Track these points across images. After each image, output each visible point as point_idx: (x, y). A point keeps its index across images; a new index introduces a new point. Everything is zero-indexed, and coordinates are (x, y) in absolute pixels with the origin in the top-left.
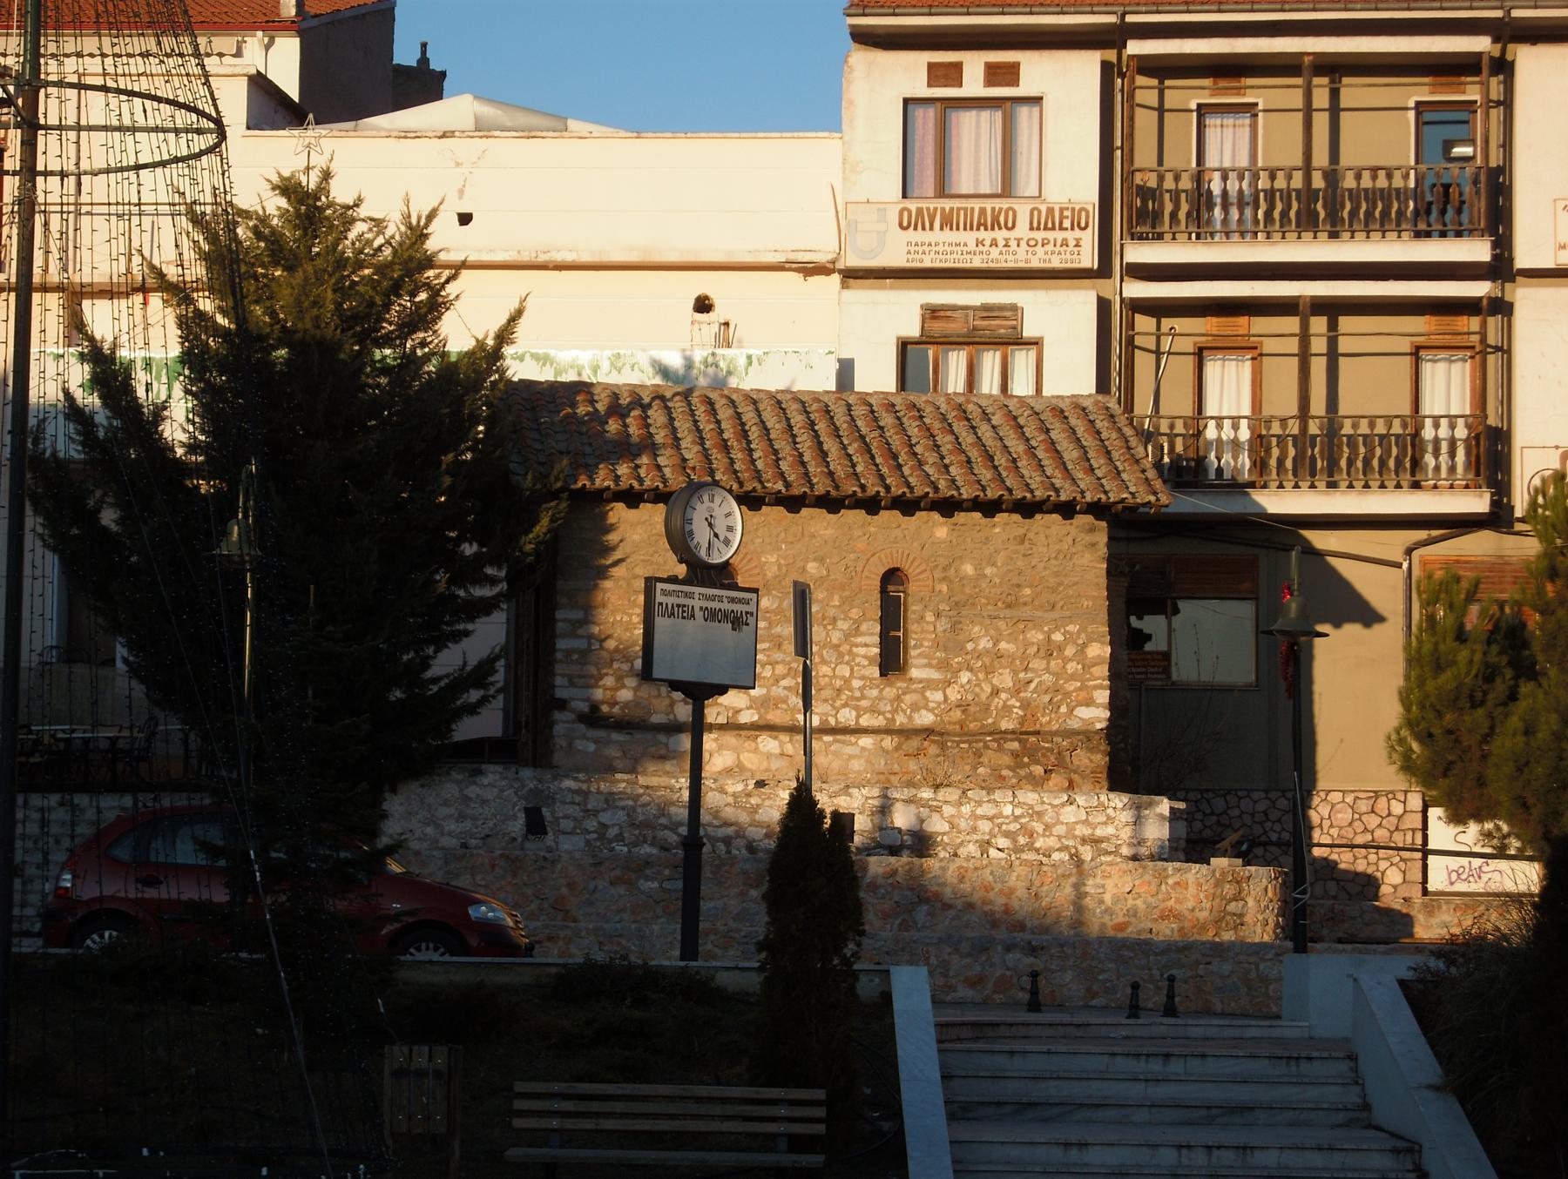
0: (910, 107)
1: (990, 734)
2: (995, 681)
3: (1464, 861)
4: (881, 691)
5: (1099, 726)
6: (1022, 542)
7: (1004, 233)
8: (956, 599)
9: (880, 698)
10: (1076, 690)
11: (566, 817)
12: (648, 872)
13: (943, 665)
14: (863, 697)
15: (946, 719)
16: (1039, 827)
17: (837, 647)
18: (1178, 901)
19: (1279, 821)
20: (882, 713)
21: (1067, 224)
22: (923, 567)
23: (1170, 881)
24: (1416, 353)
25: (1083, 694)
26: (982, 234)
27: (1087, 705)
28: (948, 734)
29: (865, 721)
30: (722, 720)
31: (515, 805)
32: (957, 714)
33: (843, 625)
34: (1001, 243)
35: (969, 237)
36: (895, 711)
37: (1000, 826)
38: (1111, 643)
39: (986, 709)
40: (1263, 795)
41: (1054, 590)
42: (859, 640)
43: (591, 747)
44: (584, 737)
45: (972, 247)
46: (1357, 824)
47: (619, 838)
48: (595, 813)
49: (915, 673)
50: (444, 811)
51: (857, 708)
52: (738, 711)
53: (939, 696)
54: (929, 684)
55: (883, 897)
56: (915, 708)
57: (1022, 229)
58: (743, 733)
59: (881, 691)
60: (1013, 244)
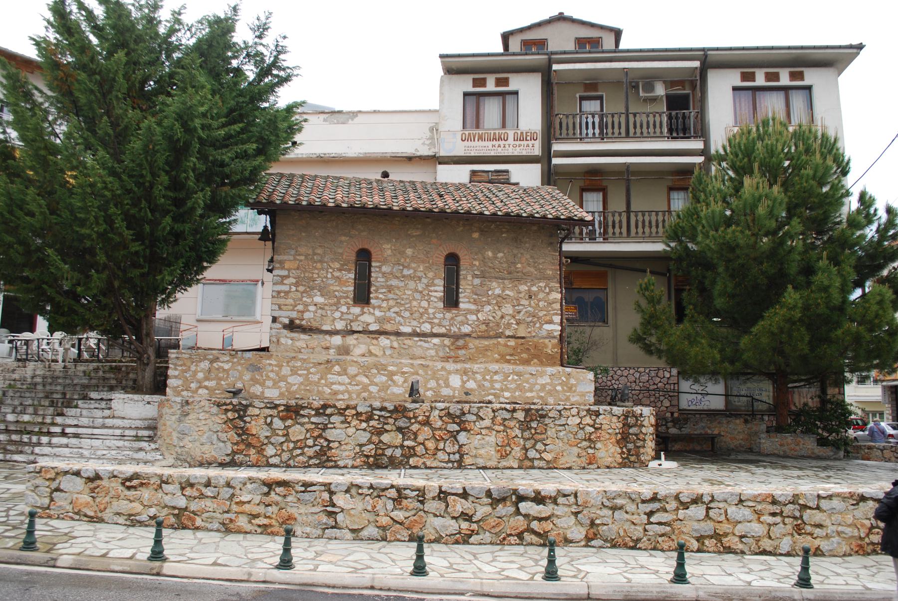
3: (694, 396)
7: (504, 142)
21: (529, 138)
26: (494, 142)
33: (425, 281)
35: (490, 144)
39: (498, 325)
42: (432, 288)
43: (290, 342)
45: (490, 147)
48: (33, 405)
49: (461, 306)
54: (470, 312)
56: (463, 323)
57: (511, 140)
58: (371, 336)
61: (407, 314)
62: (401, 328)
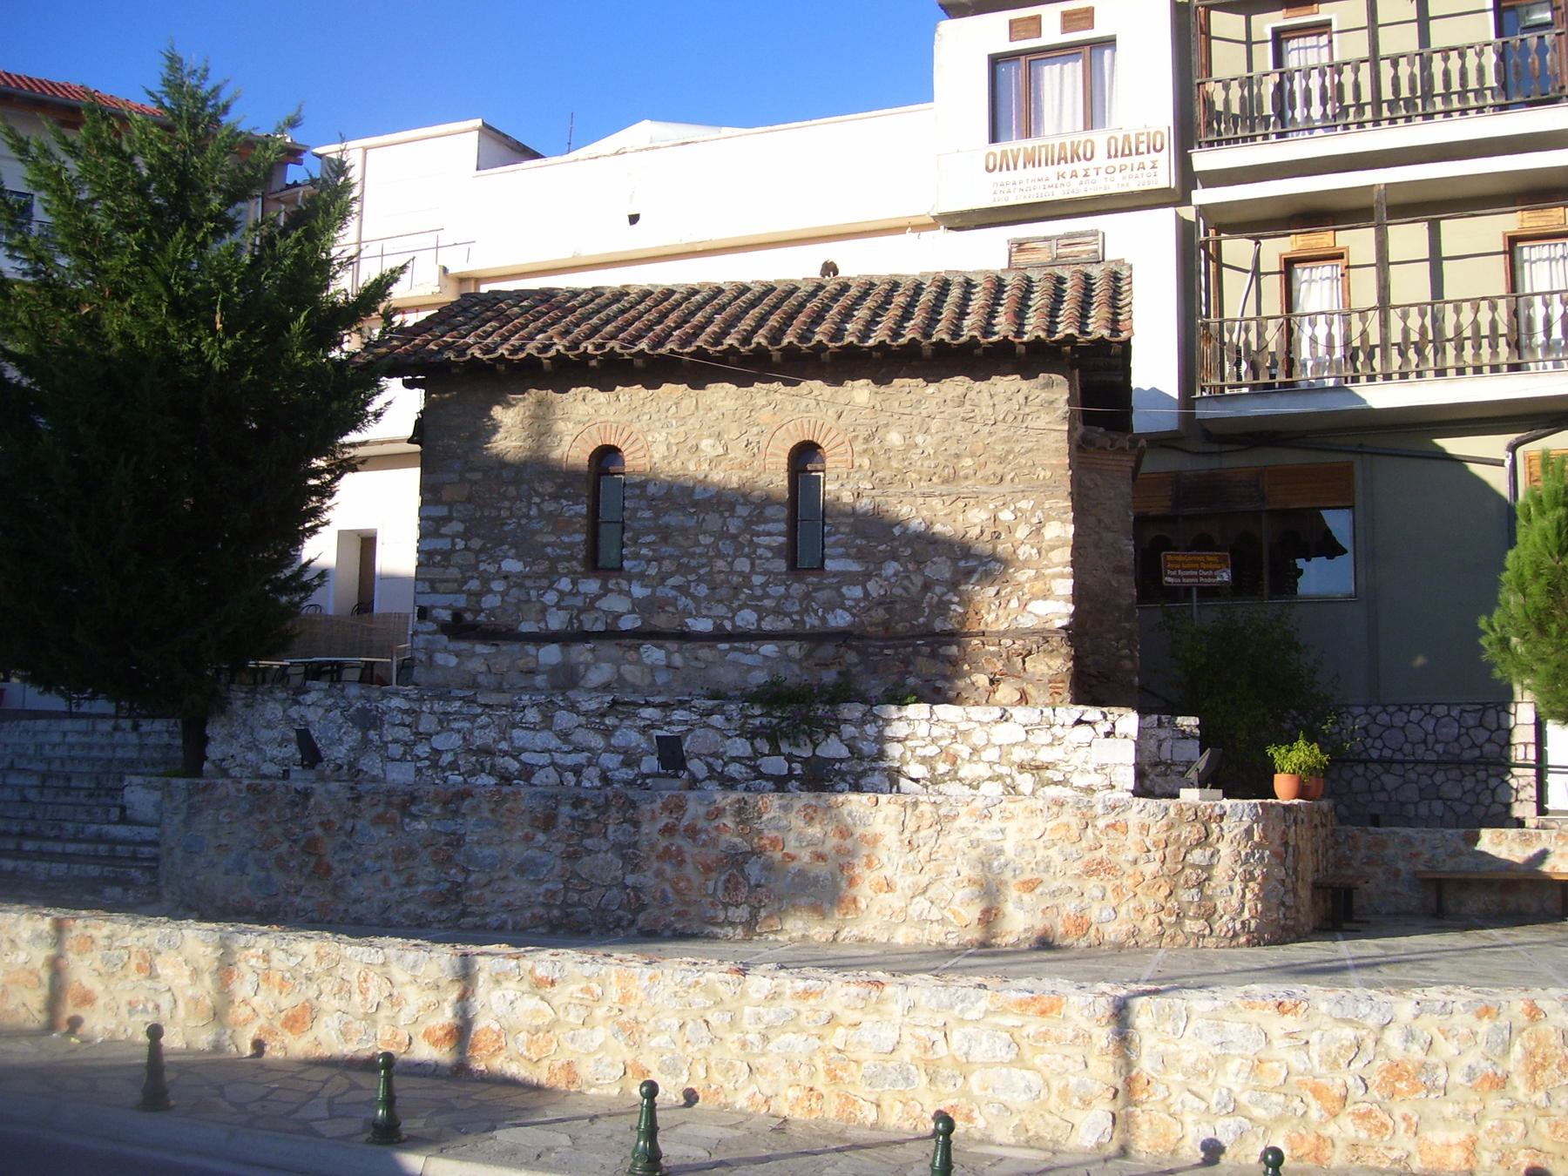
0: (1002, 69)
1: (921, 637)
2: (927, 572)
4: (788, 587)
5: (1059, 623)
6: (962, 404)
7: (1084, 164)
8: (880, 474)
9: (787, 597)
10: (1029, 580)
11: (395, 741)
12: (414, 809)
13: (860, 556)
14: (766, 596)
15: (866, 619)
16: (964, 751)
17: (734, 537)
18: (1111, 849)
19: (1380, 737)
20: (789, 615)
21: (1143, 148)
22: (839, 439)
23: (1101, 823)
24: (1513, 241)
25: (1039, 585)
27: (1045, 598)
28: (870, 638)
29: (767, 625)
30: (600, 627)
31: (340, 728)
32: (880, 614)
34: (1081, 173)
35: (1050, 171)
36: (805, 611)
37: (913, 750)
38: (1075, 521)
39: (916, 606)
40: (1363, 710)
41: (1002, 460)
42: (761, 528)
43: (453, 661)
44: (446, 650)
45: (1053, 181)
46: (1463, 739)
47: (453, 766)
50: (265, 734)
51: (756, 609)
52: (618, 616)
53: (857, 592)
55: (704, 845)
56: (830, 607)
57: (1101, 158)
59: (788, 587)
60: (1092, 173)
61: (702, 590)
62: (689, 621)
